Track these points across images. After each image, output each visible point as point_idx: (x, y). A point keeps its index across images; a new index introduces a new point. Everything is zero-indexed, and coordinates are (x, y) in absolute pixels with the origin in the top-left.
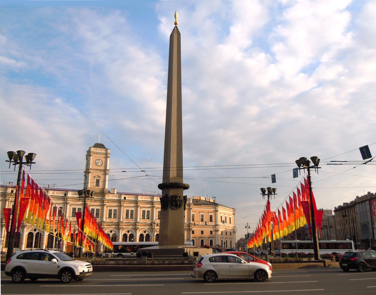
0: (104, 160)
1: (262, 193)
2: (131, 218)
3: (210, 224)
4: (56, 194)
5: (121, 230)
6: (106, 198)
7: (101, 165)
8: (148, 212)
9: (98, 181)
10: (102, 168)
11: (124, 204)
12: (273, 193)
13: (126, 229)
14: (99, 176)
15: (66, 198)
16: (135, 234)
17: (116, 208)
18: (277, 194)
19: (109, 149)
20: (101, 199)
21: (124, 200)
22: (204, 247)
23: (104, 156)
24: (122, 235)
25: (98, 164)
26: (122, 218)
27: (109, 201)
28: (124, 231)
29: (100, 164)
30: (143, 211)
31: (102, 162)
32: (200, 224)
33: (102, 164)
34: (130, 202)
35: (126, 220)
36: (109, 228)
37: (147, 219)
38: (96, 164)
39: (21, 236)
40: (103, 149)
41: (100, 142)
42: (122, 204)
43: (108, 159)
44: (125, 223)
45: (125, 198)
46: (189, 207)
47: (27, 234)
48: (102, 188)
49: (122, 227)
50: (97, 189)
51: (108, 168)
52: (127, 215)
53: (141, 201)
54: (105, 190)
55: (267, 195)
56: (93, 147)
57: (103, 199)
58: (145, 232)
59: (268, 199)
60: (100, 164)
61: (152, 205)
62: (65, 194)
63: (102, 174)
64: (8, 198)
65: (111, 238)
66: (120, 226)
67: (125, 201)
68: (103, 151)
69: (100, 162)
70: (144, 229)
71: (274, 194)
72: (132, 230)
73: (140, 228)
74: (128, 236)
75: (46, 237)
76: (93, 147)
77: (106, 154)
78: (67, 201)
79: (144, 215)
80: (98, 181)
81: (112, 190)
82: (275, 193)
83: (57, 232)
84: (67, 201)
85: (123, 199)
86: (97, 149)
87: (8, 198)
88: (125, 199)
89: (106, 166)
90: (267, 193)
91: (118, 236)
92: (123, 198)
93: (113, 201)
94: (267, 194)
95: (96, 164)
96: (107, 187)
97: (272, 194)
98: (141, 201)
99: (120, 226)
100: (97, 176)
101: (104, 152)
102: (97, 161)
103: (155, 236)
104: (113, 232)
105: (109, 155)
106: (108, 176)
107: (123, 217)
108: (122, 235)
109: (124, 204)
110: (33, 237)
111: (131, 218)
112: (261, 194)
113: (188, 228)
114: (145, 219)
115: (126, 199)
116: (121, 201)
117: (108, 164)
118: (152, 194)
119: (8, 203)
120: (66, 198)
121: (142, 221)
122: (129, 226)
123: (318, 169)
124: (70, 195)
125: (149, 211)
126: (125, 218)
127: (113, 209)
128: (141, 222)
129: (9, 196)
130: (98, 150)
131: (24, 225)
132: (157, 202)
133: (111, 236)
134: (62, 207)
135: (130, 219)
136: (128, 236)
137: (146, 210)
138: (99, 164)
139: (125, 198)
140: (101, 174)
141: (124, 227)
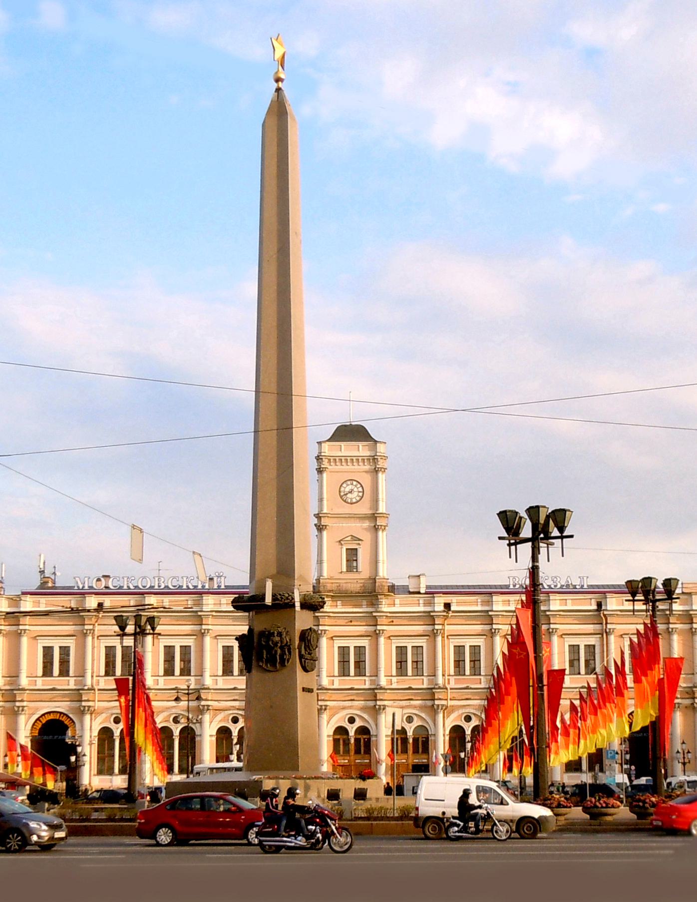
0: (366, 480)
1: (506, 535)
2: (182, 673)
3: (224, 684)
4: (571, 603)
5: (441, 715)
6: (385, 610)
7: (358, 499)
8: (65, 651)
9: (352, 554)
10: (364, 509)
11: (447, 627)
12: (555, 532)
13: (461, 711)
14: (355, 538)
15: (605, 615)
16: (374, 726)
17: (592, 641)
18: (572, 536)
19: (380, 442)
20: (424, 612)
21: (445, 614)
22: (653, 773)
23: (367, 467)
24: (444, 730)
25: (349, 495)
26: (443, 675)
27: (393, 619)
28: (454, 716)
29: (356, 494)
30: (165, 647)
31: (360, 489)
32: (39, 686)
33: (361, 494)
34: (469, 616)
35: (457, 681)
36: (344, 708)
37: (586, 674)
38: (343, 497)
39: (197, 739)
40: (361, 444)
41: (355, 419)
42: (437, 627)
43: (381, 476)
44: (99, 690)
45: (447, 606)
46: (687, 626)
47: (214, 733)
48: (370, 578)
49: (443, 705)
50: (354, 582)
51: (382, 509)
52: (459, 663)
53: (505, 614)
54: (377, 584)
55: (530, 544)
56: (329, 440)
57: (374, 614)
58: (352, 720)
59: (534, 558)
60: (356, 494)
61: (488, 627)
62: (599, 605)
63: (366, 529)
64: (91, 627)
65: (411, 741)
66: (437, 702)
67: (446, 617)
68: (361, 449)
69: (355, 489)
70: (174, 711)
71: (562, 537)
72: (366, 716)
73: (331, 708)
74: (468, 732)
75: (211, 741)
76: (329, 440)
77: (374, 459)
78: (606, 623)
79: (576, 663)
80: (352, 554)
81: (413, 581)
82: (565, 534)
83: (180, 727)
84: (606, 623)
85: (442, 608)
86: (343, 444)
87: (91, 627)
88: (450, 609)
89: (375, 501)
90: (527, 531)
91: (376, 736)
92: (439, 607)
93: (411, 618)
94: (530, 536)
95: (341, 497)
96: (383, 572)
97: (553, 535)
98: (505, 614)
99: (437, 702)
100: (349, 538)
101: (368, 453)
102: (344, 485)
103: (447, 732)
104: (417, 723)
105: (381, 464)
106: (385, 533)
107: (444, 671)
108: (444, 730)
109: (447, 627)
110: (114, 741)
111: (182, 673)
112: (500, 538)
113: (688, 702)
114: (579, 674)
115: (453, 608)
116: (433, 618)
117: (382, 495)
118: (129, 588)
119: (443, 641)
120: (605, 615)
121: (396, 682)
122: (467, 699)
123: (564, 540)
124: (613, 604)
125: (576, 648)
126: (452, 673)
127: (409, 644)
128: (218, 687)
129: (94, 620)
130: (347, 449)
131: (16, 709)
132: (562, 613)
133: (352, 733)
134: (593, 643)
135: (471, 675)
136: (468, 732)
137: (582, 642)
138: (354, 497)
139: (447, 606)
140: (360, 528)
141: (451, 703)
